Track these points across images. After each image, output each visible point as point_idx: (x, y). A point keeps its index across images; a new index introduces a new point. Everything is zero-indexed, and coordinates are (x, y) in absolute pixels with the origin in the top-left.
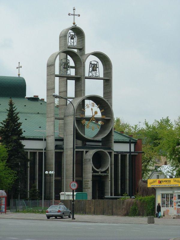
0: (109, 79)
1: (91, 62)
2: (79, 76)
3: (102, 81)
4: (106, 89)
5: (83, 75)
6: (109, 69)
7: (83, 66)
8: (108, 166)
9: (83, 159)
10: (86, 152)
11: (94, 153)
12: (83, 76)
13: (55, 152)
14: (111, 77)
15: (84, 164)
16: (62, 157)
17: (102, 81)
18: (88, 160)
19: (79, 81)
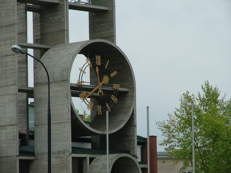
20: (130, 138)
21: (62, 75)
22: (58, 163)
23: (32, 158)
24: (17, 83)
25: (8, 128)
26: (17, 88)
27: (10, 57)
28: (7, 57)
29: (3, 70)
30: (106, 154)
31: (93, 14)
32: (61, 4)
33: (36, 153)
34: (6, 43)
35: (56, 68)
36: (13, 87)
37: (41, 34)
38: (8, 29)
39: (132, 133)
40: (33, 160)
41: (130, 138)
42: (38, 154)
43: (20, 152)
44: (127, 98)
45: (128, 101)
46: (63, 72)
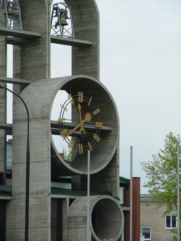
0: (91, 45)
1: (56, 4)
2: (38, 34)
3: (69, 48)
4: (82, 66)
5: (48, 32)
6: (90, 22)
7: (47, 12)
8: (120, 233)
9: (65, 218)
10: (71, 201)
11: (94, 204)
12: (47, 34)
13: (91, 194)
14: (97, 40)
15: (65, 227)
16: (63, 209)
17: (69, 48)
18: (81, 219)
19: (39, 44)
20: (113, 179)
23: (9, 198)
32: (43, 38)
39: (114, 174)
41: (113, 179)
44: (109, 137)
45: (111, 140)
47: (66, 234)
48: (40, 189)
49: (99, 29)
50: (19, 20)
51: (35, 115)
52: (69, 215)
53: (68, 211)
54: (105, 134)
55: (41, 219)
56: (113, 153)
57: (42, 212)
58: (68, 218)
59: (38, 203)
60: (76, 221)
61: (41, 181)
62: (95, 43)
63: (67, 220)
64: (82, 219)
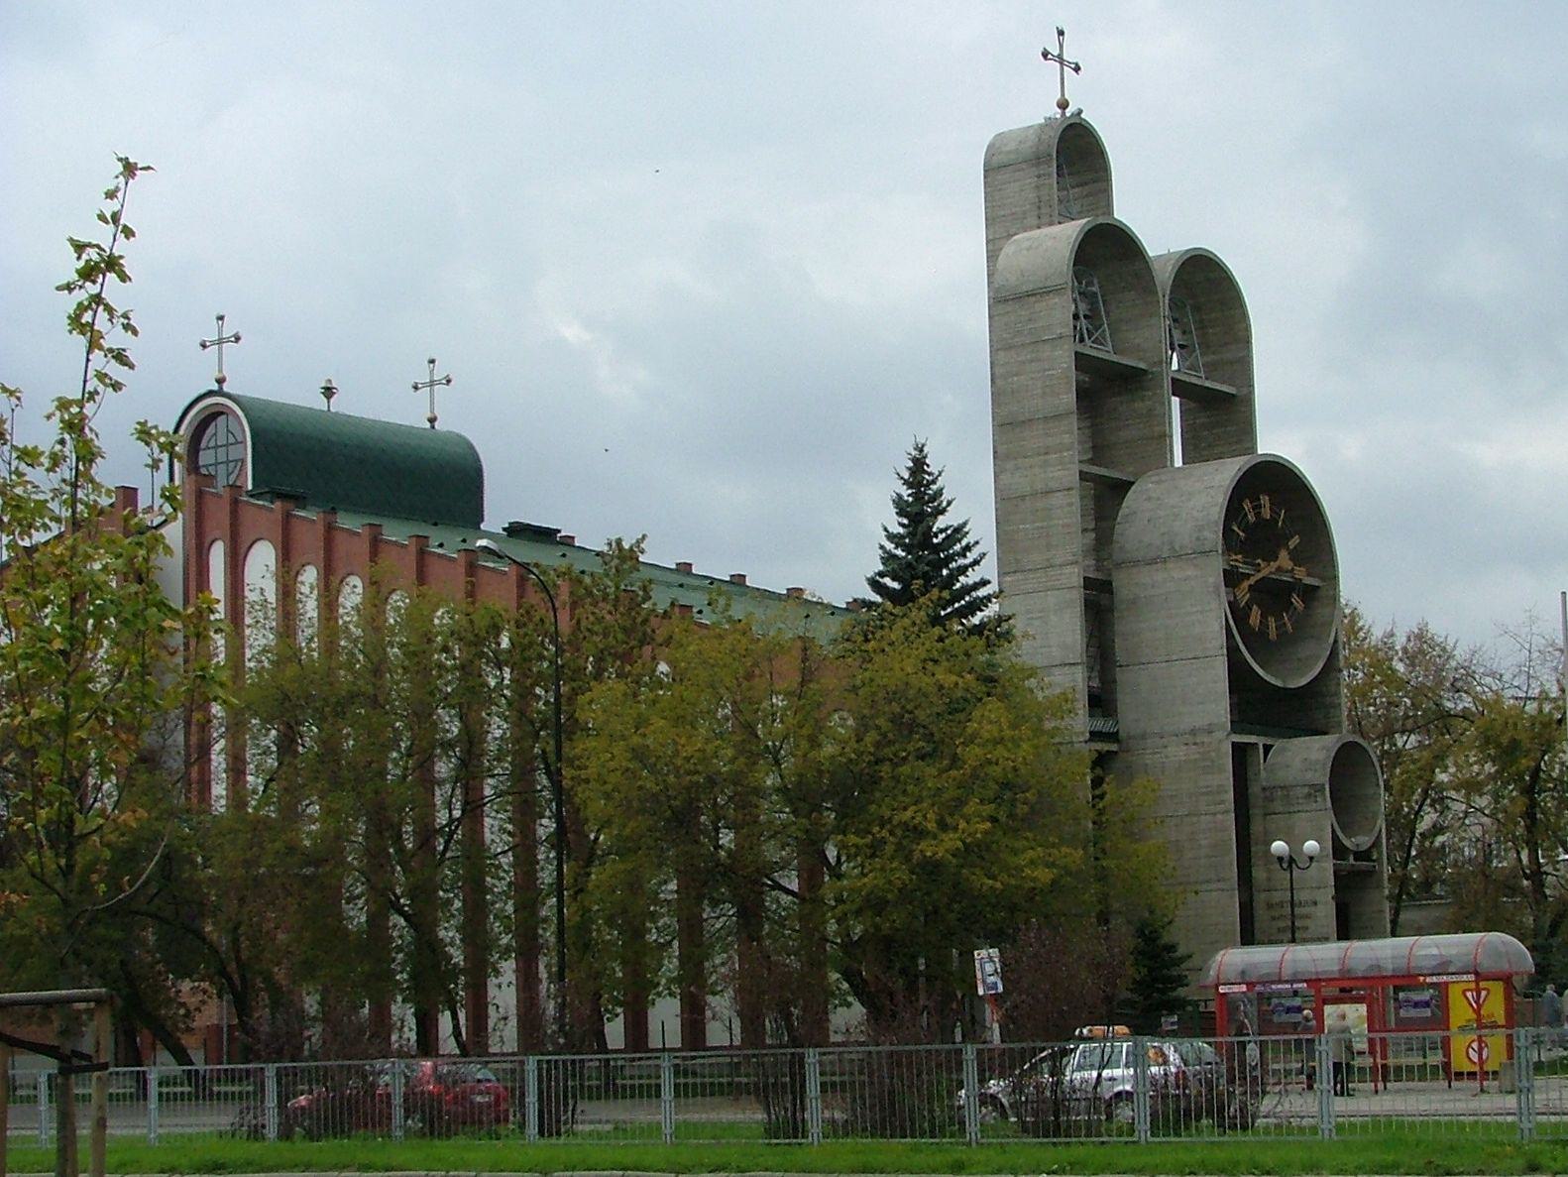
2: (1142, 366)
8: (1379, 821)
9: (1254, 789)
20: (1328, 700)
21: (1198, 539)
22: (1192, 757)
23: (1114, 747)
24: (1080, 559)
25: (1056, 671)
26: (1082, 574)
27: (1059, 494)
28: (1051, 495)
29: (1038, 528)
30: (1234, 730)
31: (1193, 405)
32: (1152, 373)
33: (1122, 735)
34: (1045, 461)
35: (1178, 523)
36: (1068, 570)
37: (1093, 447)
38: (1051, 425)
39: (1333, 689)
40: (1116, 752)
41: (1328, 700)
42: (1129, 738)
43: (1091, 733)
44: (1316, 603)
45: (1321, 612)
46: (1199, 531)
47: (1261, 829)
48: (1200, 722)
49: (268, 403)
50: (1104, 331)
51: (1177, 548)
52: (266, 752)
53: (1263, 774)
54: (1309, 593)
55: (1207, 794)
56: (1331, 640)
57: (1210, 777)
58: (1264, 789)
59: (1197, 756)
60: (1288, 795)
61: (1202, 703)
62: (1245, 391)
63: (1262, 795)
64: (1306, 790)
